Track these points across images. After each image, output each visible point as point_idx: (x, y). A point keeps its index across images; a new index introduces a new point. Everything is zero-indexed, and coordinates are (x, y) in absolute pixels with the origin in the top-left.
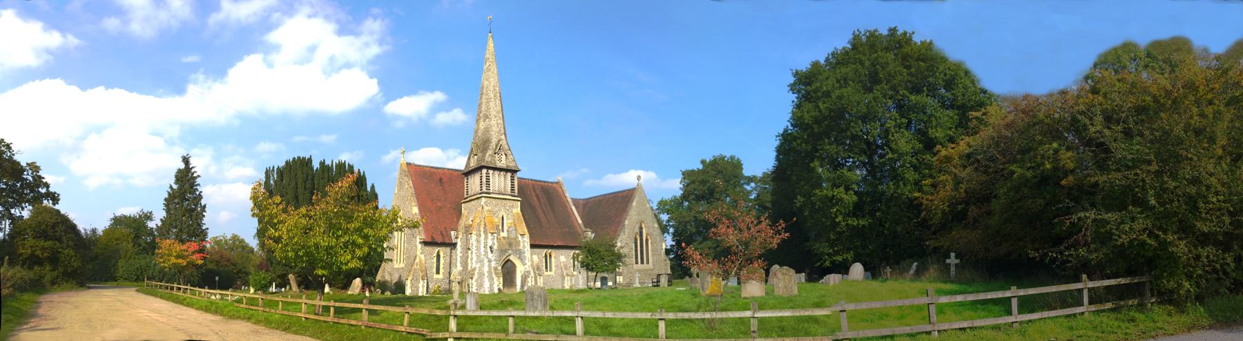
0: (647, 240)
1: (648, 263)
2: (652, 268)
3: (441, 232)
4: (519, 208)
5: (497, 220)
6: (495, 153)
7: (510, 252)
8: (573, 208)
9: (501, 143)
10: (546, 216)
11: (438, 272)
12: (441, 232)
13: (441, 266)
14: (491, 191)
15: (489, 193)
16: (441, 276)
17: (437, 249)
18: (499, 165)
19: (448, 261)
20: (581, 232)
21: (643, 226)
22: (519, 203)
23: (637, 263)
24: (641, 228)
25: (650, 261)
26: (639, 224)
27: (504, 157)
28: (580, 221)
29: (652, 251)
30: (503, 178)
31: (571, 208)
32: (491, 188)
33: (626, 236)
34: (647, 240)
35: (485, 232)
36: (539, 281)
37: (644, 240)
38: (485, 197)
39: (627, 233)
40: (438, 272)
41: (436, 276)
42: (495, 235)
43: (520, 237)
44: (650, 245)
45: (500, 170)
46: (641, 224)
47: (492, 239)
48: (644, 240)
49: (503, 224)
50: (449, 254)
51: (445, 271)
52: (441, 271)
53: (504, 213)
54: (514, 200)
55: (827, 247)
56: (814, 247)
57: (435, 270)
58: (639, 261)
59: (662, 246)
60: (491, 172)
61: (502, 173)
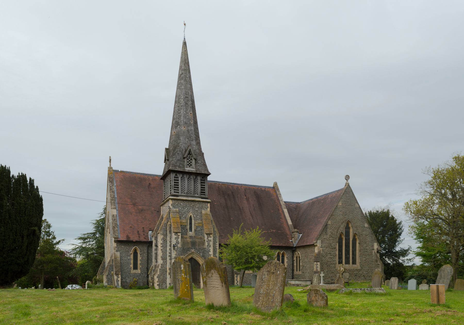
0: (354, 240)
1: (354, 262)
2: (359, 268)
3: (138, 232)
4: (209, 209)
5: (185, 221)
6: (184, 158)
7: (193, 250)
8: (286, 211)
9: (190, 148)
10: (252, 217)
11: (135, 267)
12: (138, 232)
13: (139, 262)
14: (180, 194)
15: (177, 196)
16: (139, 271)
17: (278, 251)
18: (188, 169)
19: (145, 258)
20: (288, 232)
21: (350, 226)
22: (209, 205)
23: (340, 262)
24: (347, 228)
25: (358, 260)
26: (345, 224)
27: (193, 161)
28: (290, 222)
29: (360, 251)
30: (192, 182)
31: (283, 212)
32: (180, 191)
33: (328, 236)
34: (354, 240)
35: (170, 232)
36: (235, 278)
37: (351, 240)
38: (172, 199)
39: (329, 233)
40: (135, 267)
41: (133, 271)
42: (179, 234)
43: (206, 236)
44: (358, 245)
45: (190, 173)
46: (348, 224)
47: (176, 238)
48: (351, 240)
49: (191, 224)
50: (146, 251)
51: (142, 267)
52: (139, 266)
53: (191, 214)
54: (203, 202)
55: (398, 229)
56: (92, 258)
57: (132, 266)
58: (344, 261)
59: (373, 246)
60: (180, 176)
61: (192, 177)
